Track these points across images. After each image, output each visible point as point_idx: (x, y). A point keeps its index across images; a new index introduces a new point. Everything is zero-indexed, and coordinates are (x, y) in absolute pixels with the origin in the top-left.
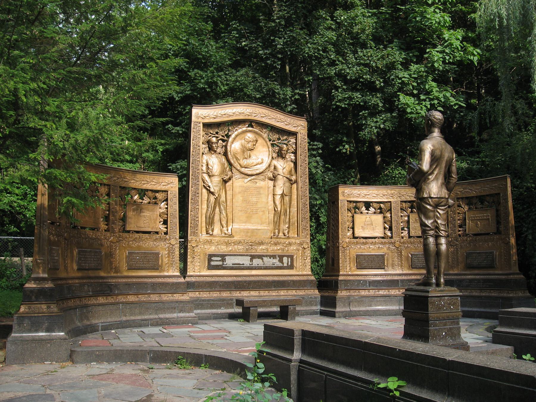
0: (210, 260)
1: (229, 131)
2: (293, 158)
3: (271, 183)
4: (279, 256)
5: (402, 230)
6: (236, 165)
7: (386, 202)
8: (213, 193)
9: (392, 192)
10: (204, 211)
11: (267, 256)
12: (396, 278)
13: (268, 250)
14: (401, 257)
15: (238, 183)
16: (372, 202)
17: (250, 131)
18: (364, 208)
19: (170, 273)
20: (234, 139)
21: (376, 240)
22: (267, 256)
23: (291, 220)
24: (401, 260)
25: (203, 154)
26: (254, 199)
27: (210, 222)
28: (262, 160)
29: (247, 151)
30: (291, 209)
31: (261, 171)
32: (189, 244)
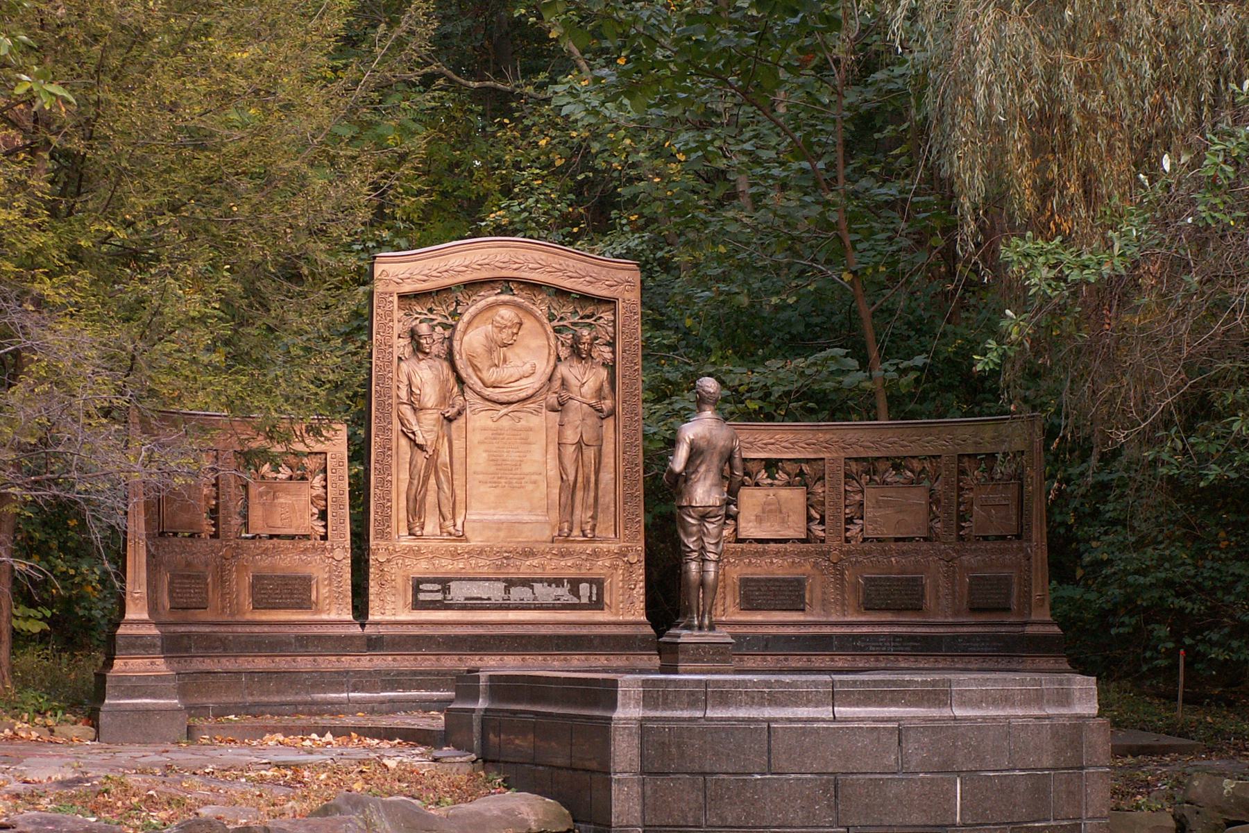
0: (416, 590)
1: (458, 304)
2: (609, 356)
3: (555, 417)
4: (570, 581)
5: (846, 523)
6: (473, 380)
7: (815, 460)
8: (421, 447)
9: (828, 437)
10: (404, 486)
11: (541, 581)
12: (827, 630)
13: (544, 569)
14: (842, 585)
15: (480, 420)
16: (781, 460)
17: (505, 303)
18: (763, 474)
19: (333, 616)
20: (469, 323)
21: (787, 546)
22: (541, 581)
23: (601, 501)
24: (843, 592)
25: (400, 358)
26: (514, 456)
27: (416, 510)
28: (534, 366)
29: (499, 347)
30: (601, 475)
31: (530, 392)
32: (372, 557)
